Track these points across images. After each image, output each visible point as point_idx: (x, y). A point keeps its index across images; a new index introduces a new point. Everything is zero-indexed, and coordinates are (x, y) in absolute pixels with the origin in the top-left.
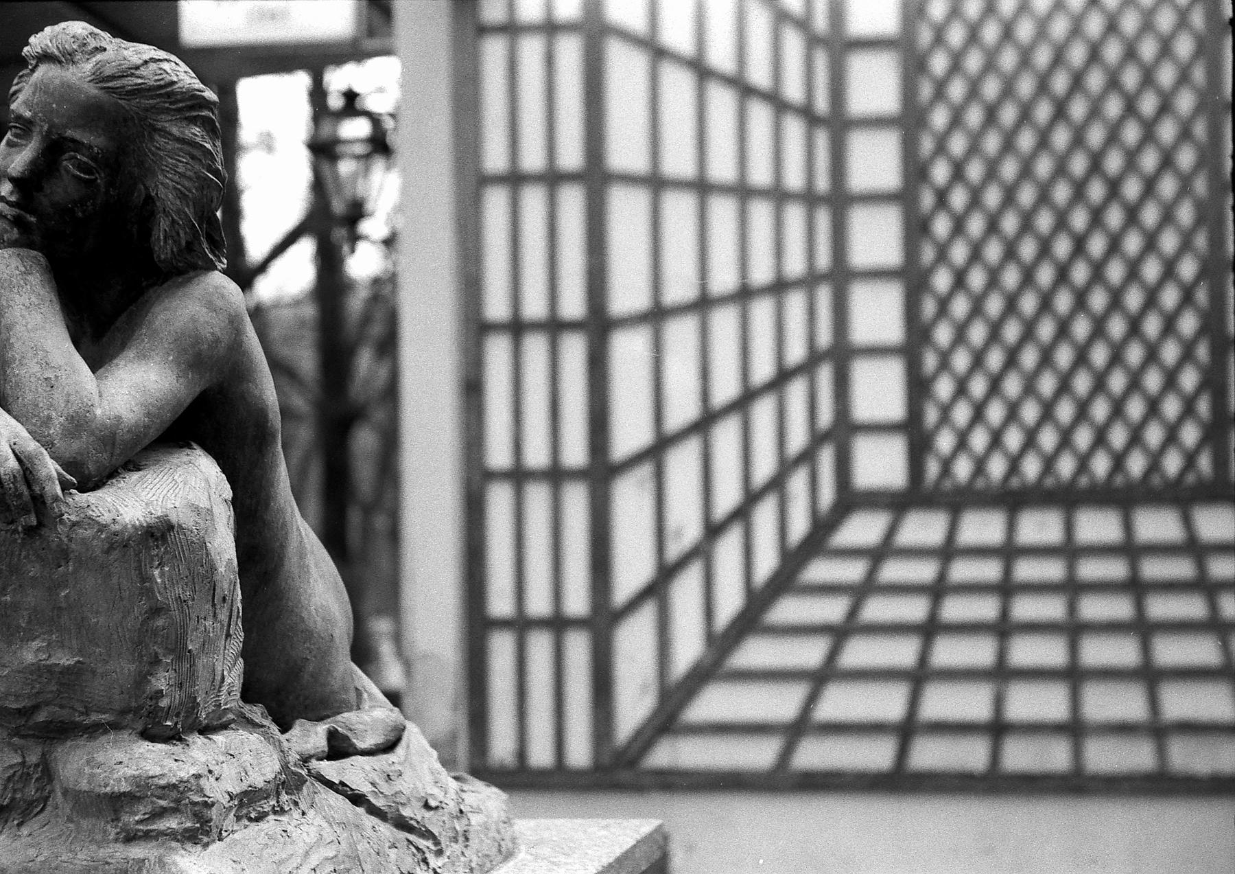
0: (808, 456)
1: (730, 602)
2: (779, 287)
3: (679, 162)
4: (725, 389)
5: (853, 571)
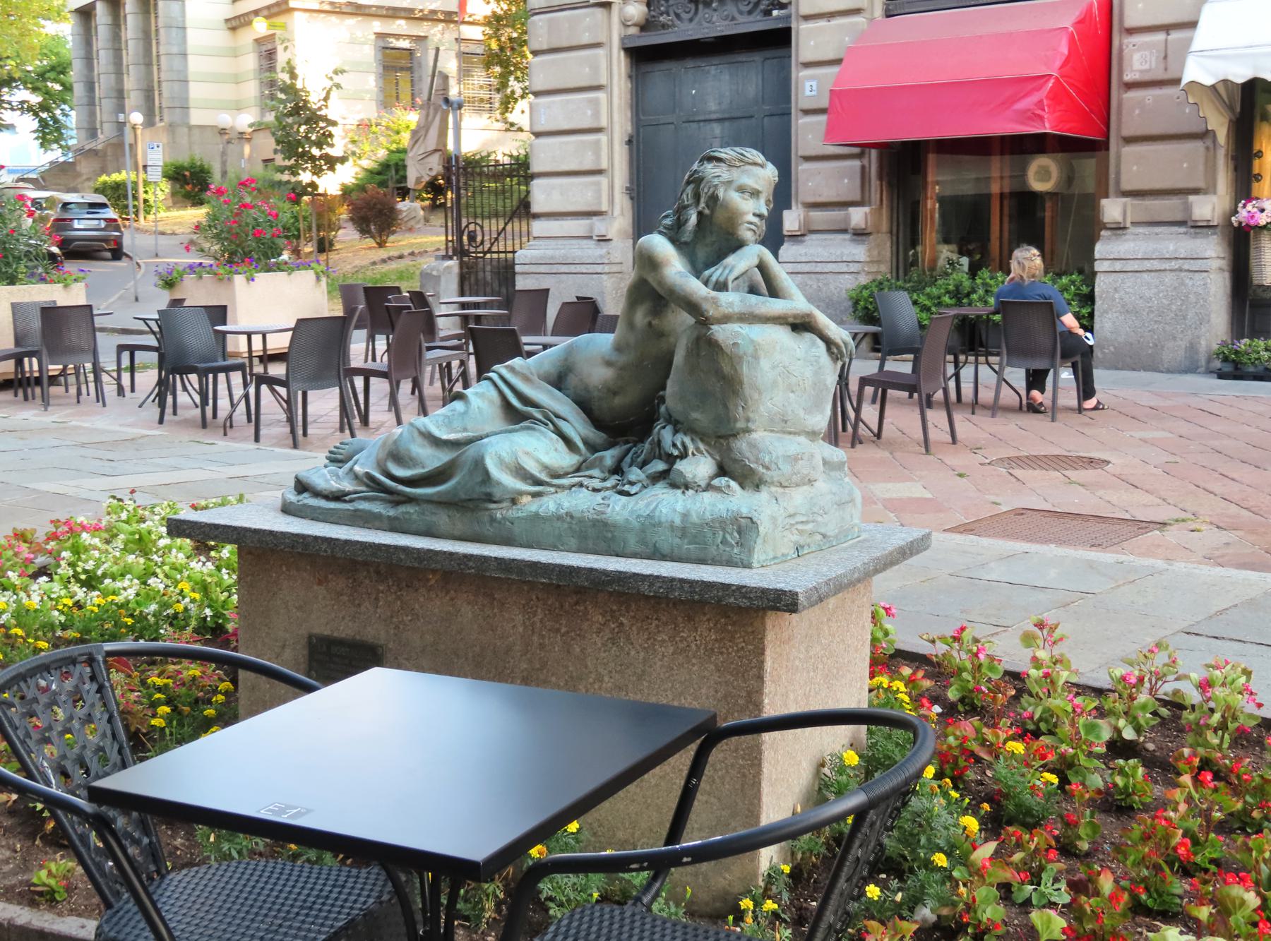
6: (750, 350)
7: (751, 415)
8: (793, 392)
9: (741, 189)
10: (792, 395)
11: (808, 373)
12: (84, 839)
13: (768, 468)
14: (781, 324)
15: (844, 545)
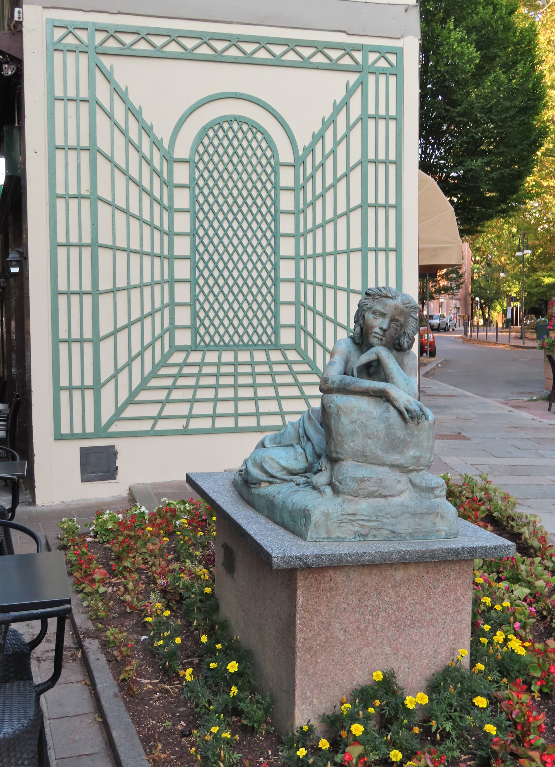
0: (161, 337)
1: (123, 396)
2: (313, 257)
3: (330, 293)
4: (147, 309)
5: (174, 371)
6: (335, 411)
7: (339, 450)
8: (369, 438)
9: (374, 313)
10: (369, 440)
11: (381, 428)
12: (504, 672)
13: (341, 483)
14: (365, 396)
15: (414, 541)
